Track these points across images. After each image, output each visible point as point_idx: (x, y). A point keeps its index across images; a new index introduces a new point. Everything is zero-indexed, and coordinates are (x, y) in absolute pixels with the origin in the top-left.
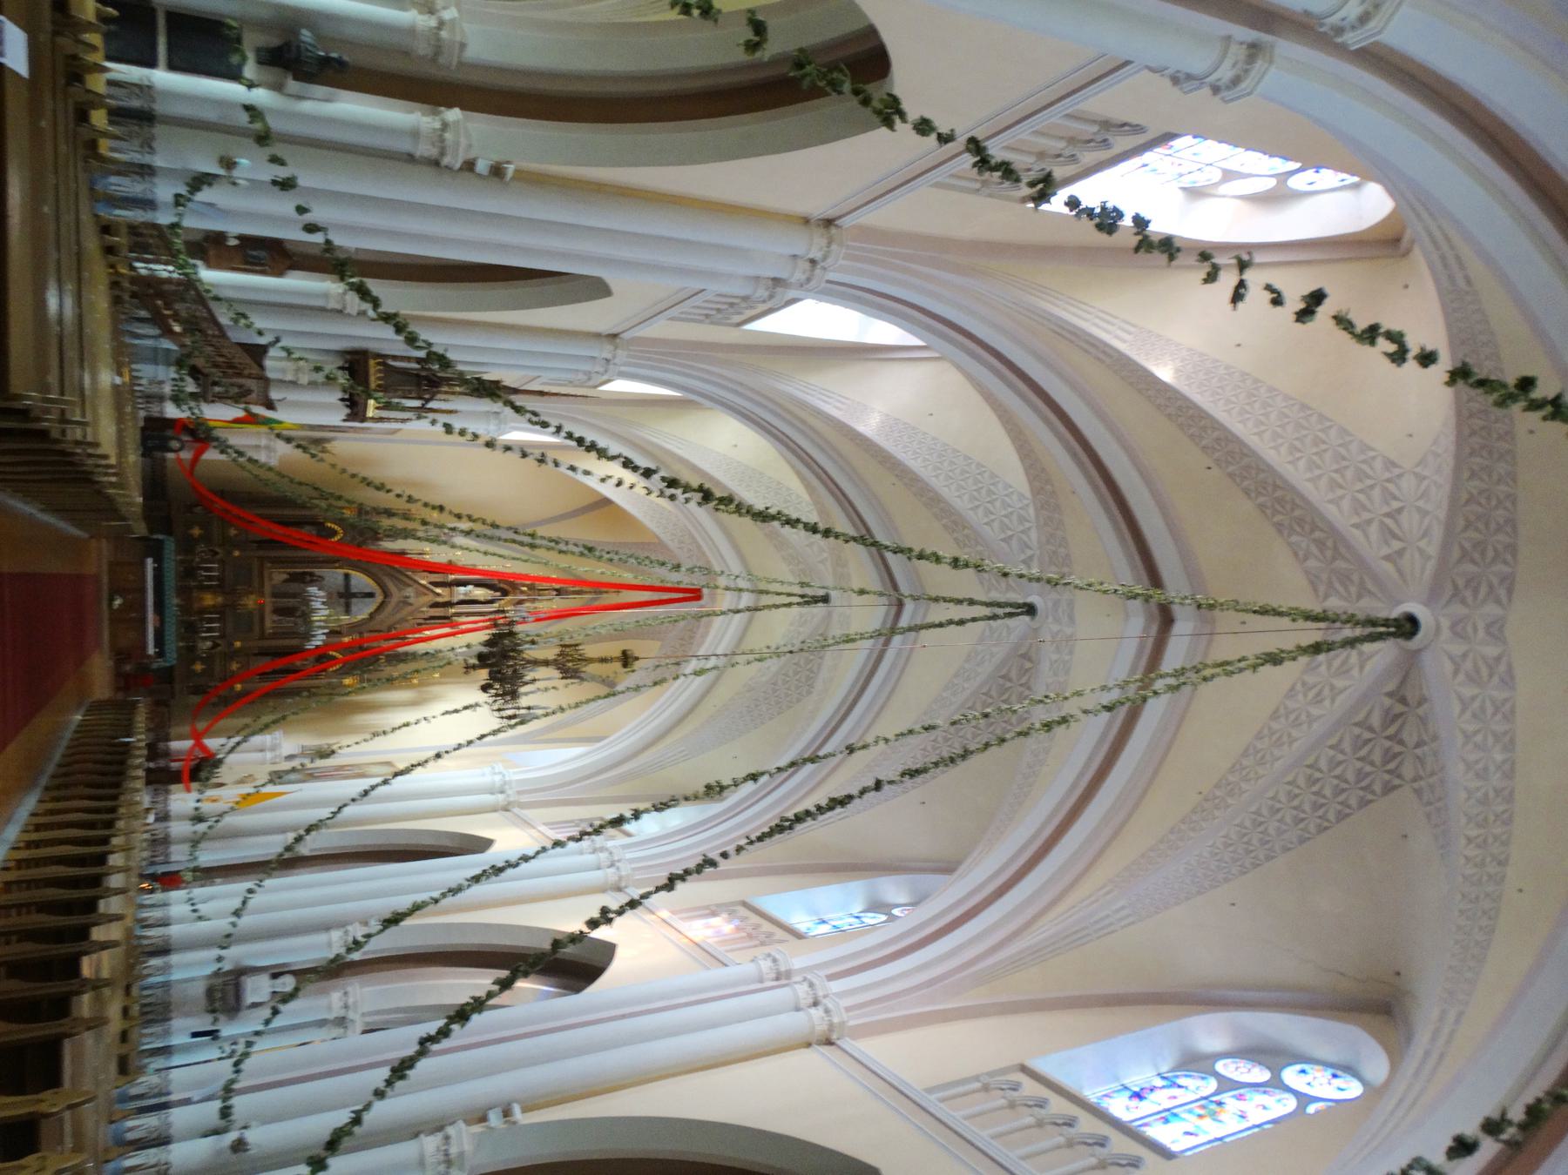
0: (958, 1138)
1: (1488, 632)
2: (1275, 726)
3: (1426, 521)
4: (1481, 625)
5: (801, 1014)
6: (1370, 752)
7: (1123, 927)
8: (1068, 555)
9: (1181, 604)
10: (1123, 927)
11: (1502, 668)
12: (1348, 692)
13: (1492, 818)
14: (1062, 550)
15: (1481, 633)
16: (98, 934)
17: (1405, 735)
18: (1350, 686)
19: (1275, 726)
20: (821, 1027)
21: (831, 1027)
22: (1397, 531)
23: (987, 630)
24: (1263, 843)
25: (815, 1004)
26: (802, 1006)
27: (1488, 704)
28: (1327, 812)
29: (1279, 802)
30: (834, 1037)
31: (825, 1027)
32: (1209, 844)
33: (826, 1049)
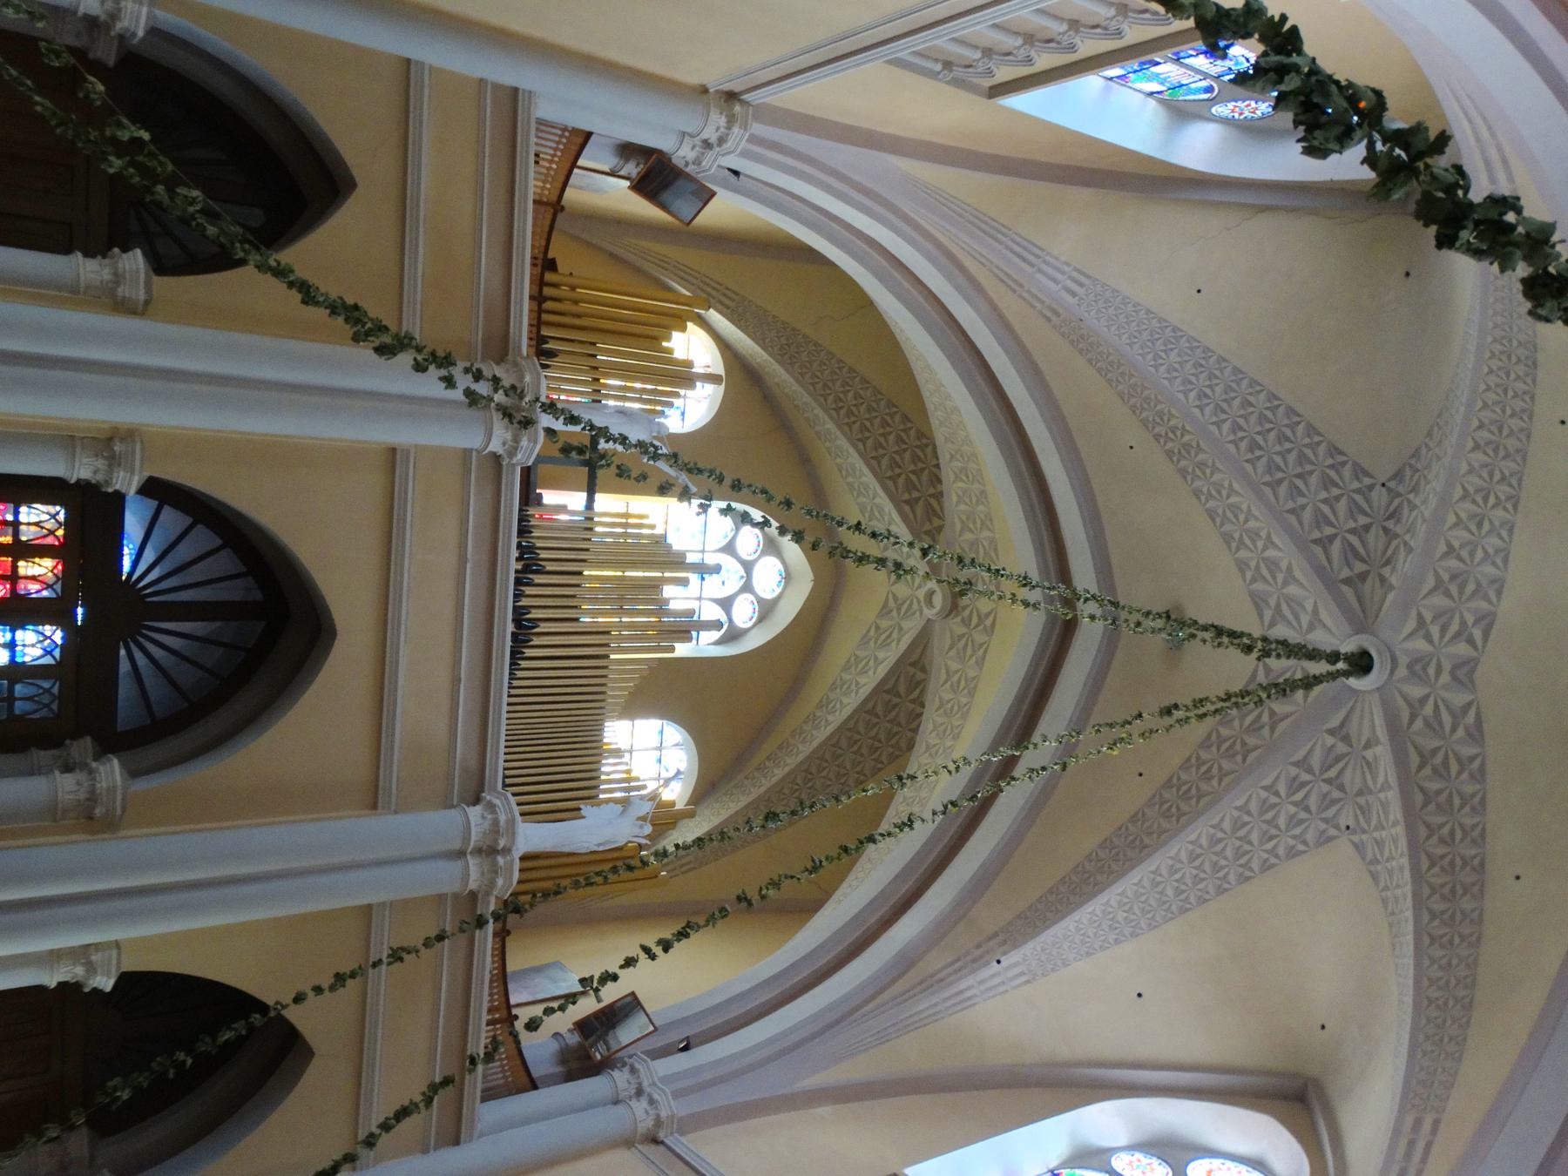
0: (969, 6)
1: (1455, 678)
2: (1204, 755)
3: (1396, 502)
4: (1447, 666)
5: (620, 1109)
6: (1306, 797)
7: (1014, 988)
8: (983, 493)
9: (1100, 726)
10: (1014, 988)
11: (1470, 718)
12: (1293, 718)
13: (1453, 982)
14: (972, 465)
15: (1445, 678)
16: (127, 295)
17: (1346, 779)
18: (1296, 712)
19: (1204, 755)
20: (645, 1124)
21: (658, 1122)
22: (1361, 550)
23: (873, 629)
24: (1178, 892)
25: (639, 1092)
26: (622, 1095)
27: (1458, 860)
28: (1249, 832)
29: (1204, 872)
30: (661, 1135)
31: (650, 1123)
32: (1119, 891)
33: (651, 1150)
